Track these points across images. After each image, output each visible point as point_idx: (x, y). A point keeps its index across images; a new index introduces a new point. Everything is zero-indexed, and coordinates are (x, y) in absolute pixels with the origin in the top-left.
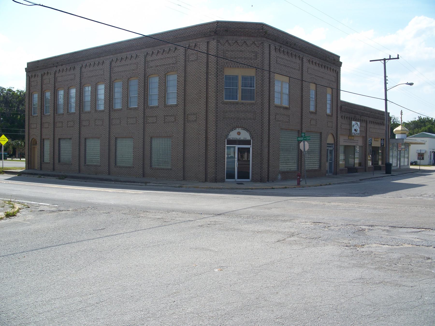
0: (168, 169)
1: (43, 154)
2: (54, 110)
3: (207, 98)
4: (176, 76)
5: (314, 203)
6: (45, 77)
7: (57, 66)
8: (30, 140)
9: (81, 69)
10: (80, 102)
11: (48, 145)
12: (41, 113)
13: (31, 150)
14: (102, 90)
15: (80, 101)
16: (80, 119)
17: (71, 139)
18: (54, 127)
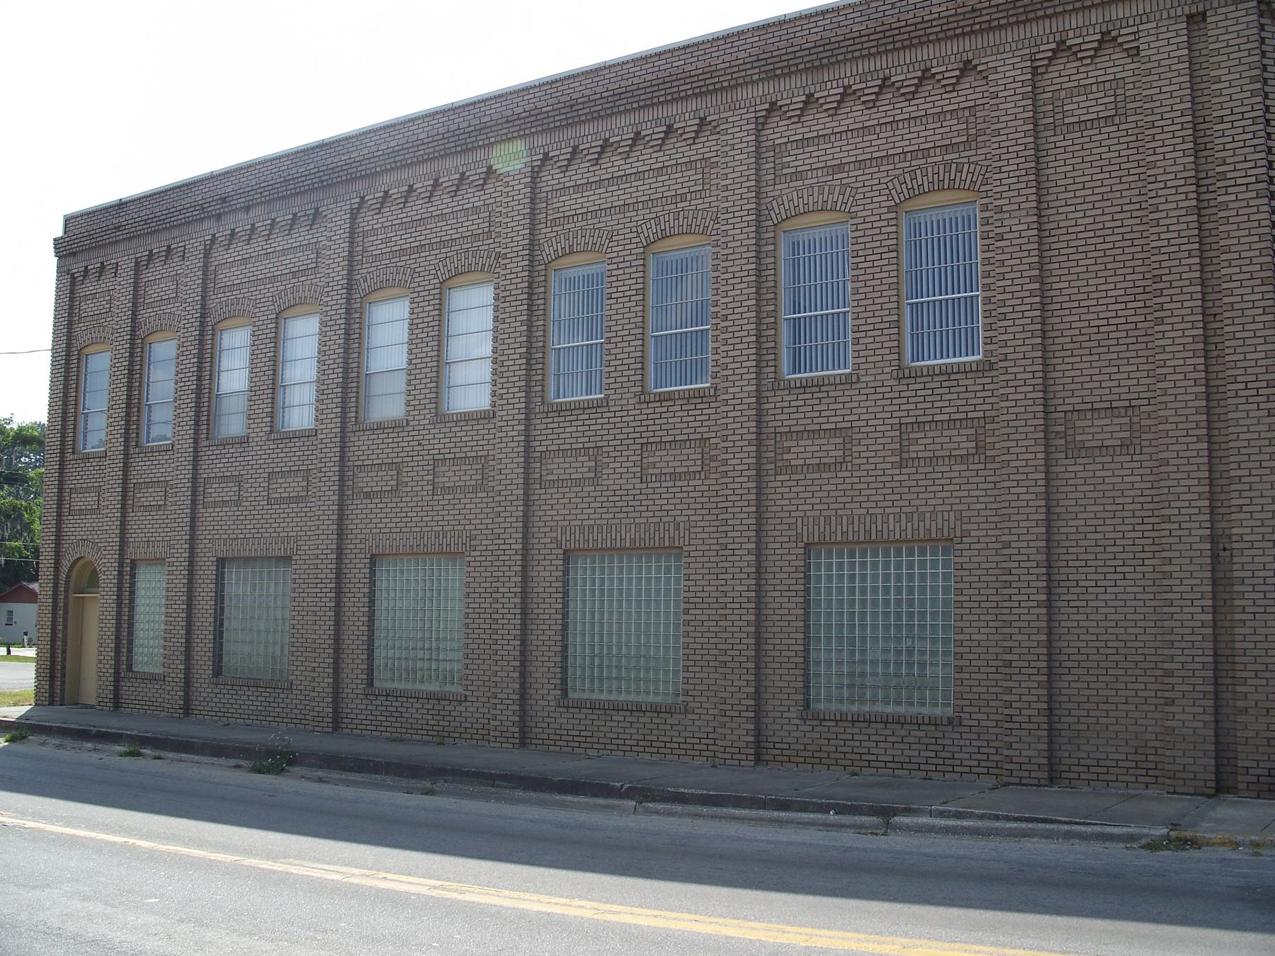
0: (934, 722)
1: (131, 633)
2: (197, 423)
3: (1208, 317)
4: (407, 303)
5: (576, 799)
6: (157, 269)
7: (218, 217)
8: (66, 565)
9: (353, 218)
10: (346, 378)
11: (154, 595)
12: (127, 440)
13: (66, 612)
14: (304, 338)
15: (346, 370)
16: (342, 458)
17: (287, 560)
18: (194, 502)
